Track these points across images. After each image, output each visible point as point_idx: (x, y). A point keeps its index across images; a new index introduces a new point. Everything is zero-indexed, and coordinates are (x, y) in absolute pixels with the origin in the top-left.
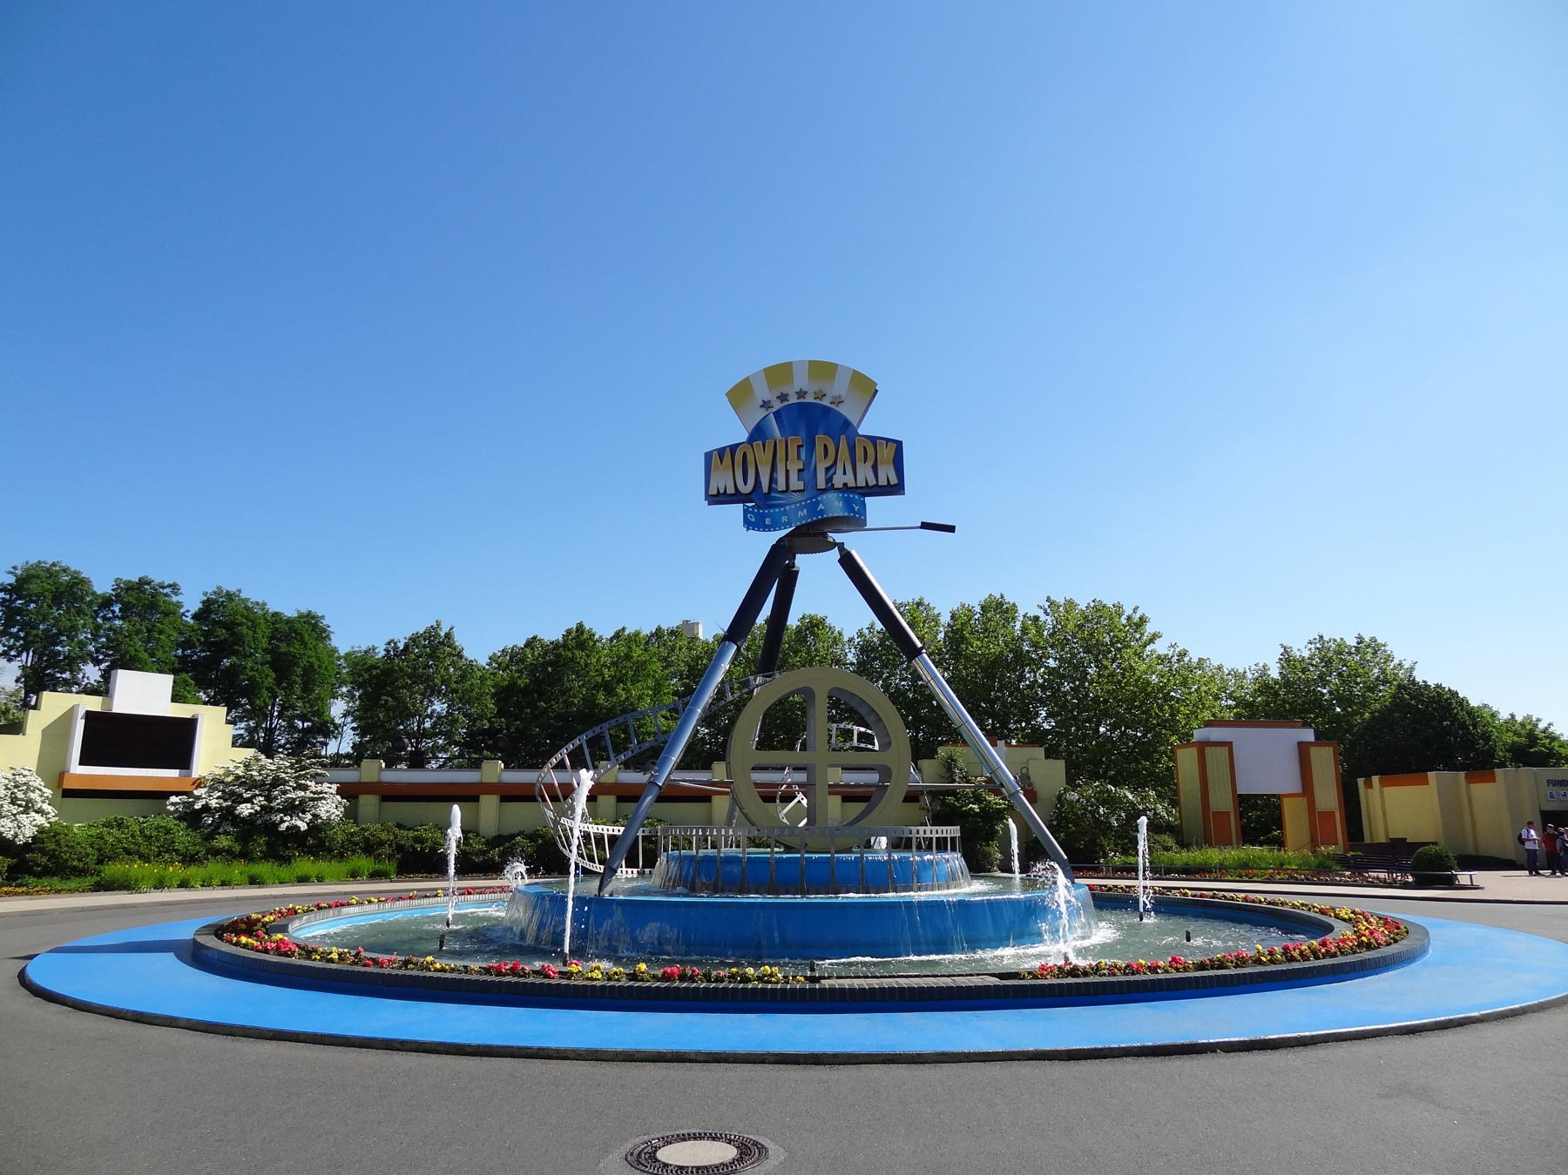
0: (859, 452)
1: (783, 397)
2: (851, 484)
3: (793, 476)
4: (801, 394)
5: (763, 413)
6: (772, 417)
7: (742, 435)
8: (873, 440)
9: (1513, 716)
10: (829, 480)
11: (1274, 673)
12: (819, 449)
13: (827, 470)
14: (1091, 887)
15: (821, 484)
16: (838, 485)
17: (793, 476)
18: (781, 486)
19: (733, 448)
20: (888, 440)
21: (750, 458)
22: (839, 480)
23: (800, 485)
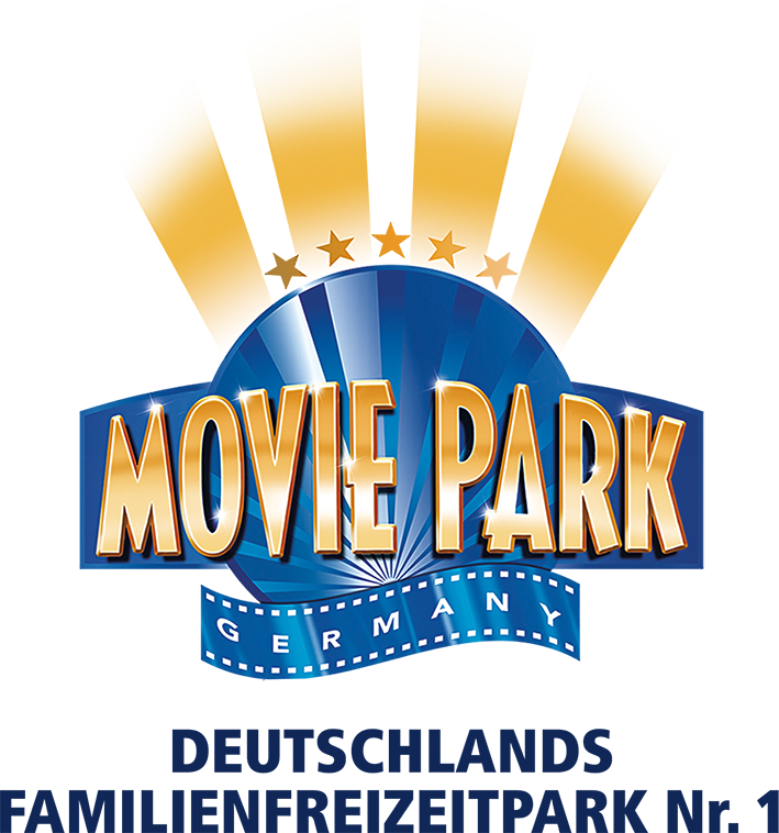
0: (571, 437)
1: (336, 249)
2: (541, 542)
3: (363, 500)
4: (390, 239)
5: (275, 289)
6: (295, 307)
7: (201, 358)
8: (611, 398)
9: (391, 226)
10: (473, 526)
11: (384, 232)
12: (448, 431)
13: (467, 491)
14: (568, 637)
15: (449, 536)
16: (500, 542)
17: (363, 500)
18: (325, 540)
19: (178, 398)
20: (657, 407)
21: (227, 436)
22: (502, 523)
23: (381, 536)
